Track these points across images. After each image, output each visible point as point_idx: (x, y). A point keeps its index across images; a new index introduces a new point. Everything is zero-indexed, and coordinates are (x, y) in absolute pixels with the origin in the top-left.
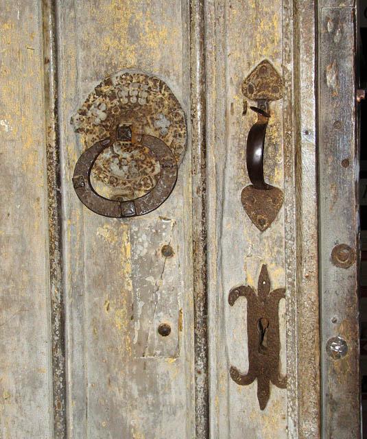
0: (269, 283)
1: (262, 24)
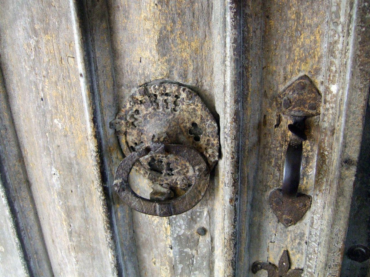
0: (290, 263)
1: (302, 36)
